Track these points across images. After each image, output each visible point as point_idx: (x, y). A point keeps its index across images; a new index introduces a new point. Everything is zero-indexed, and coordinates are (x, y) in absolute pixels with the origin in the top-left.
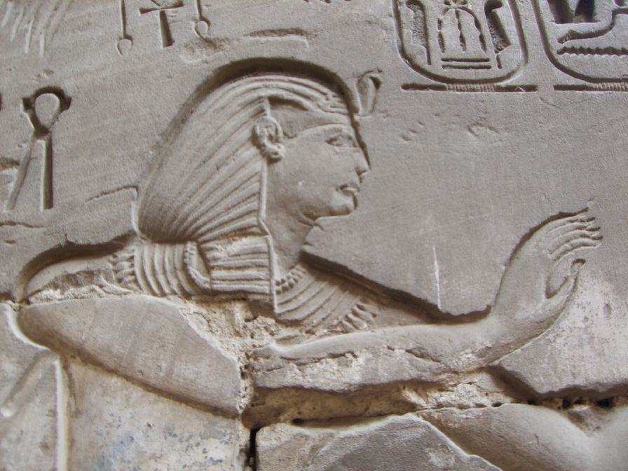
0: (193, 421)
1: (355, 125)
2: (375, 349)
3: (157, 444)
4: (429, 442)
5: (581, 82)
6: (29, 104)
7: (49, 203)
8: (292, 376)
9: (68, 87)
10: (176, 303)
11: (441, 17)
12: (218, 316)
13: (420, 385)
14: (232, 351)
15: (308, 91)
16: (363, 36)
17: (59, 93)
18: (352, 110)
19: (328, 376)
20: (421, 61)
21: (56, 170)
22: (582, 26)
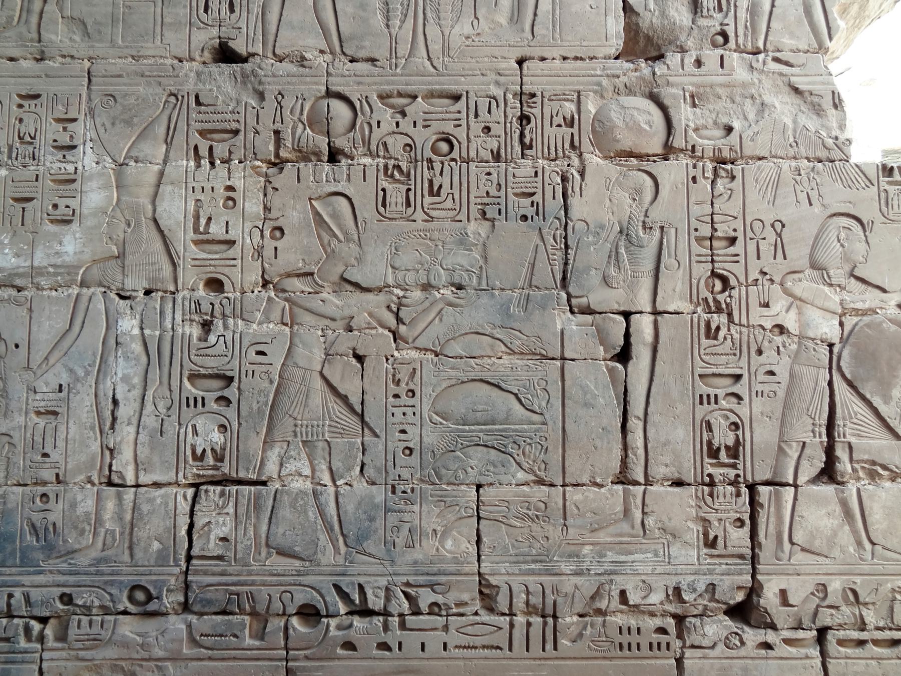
0: (829, 315)
1: (865, 236)
2: (871, 298)
3: (821, 321)
4: (884, 321)
5: (271, 38)
6: (773, 226)
7: (785, 258)
8: (852, 306)
9: (783, 220)
10: (822, 286)
11: (141, 294)
12: (832, 289)
13: (881, 308)
14: (837, 299)
15: (859, 179)
16: (569, 157)
17: (780, 221)
18: (865, 231)
19: (859, 305)
20: (886, 214)
21: (785, 248)
22: (436, 199)
